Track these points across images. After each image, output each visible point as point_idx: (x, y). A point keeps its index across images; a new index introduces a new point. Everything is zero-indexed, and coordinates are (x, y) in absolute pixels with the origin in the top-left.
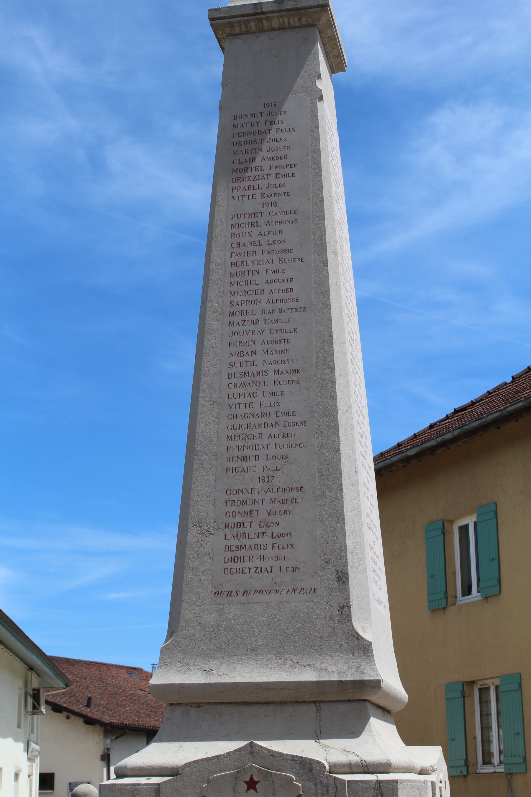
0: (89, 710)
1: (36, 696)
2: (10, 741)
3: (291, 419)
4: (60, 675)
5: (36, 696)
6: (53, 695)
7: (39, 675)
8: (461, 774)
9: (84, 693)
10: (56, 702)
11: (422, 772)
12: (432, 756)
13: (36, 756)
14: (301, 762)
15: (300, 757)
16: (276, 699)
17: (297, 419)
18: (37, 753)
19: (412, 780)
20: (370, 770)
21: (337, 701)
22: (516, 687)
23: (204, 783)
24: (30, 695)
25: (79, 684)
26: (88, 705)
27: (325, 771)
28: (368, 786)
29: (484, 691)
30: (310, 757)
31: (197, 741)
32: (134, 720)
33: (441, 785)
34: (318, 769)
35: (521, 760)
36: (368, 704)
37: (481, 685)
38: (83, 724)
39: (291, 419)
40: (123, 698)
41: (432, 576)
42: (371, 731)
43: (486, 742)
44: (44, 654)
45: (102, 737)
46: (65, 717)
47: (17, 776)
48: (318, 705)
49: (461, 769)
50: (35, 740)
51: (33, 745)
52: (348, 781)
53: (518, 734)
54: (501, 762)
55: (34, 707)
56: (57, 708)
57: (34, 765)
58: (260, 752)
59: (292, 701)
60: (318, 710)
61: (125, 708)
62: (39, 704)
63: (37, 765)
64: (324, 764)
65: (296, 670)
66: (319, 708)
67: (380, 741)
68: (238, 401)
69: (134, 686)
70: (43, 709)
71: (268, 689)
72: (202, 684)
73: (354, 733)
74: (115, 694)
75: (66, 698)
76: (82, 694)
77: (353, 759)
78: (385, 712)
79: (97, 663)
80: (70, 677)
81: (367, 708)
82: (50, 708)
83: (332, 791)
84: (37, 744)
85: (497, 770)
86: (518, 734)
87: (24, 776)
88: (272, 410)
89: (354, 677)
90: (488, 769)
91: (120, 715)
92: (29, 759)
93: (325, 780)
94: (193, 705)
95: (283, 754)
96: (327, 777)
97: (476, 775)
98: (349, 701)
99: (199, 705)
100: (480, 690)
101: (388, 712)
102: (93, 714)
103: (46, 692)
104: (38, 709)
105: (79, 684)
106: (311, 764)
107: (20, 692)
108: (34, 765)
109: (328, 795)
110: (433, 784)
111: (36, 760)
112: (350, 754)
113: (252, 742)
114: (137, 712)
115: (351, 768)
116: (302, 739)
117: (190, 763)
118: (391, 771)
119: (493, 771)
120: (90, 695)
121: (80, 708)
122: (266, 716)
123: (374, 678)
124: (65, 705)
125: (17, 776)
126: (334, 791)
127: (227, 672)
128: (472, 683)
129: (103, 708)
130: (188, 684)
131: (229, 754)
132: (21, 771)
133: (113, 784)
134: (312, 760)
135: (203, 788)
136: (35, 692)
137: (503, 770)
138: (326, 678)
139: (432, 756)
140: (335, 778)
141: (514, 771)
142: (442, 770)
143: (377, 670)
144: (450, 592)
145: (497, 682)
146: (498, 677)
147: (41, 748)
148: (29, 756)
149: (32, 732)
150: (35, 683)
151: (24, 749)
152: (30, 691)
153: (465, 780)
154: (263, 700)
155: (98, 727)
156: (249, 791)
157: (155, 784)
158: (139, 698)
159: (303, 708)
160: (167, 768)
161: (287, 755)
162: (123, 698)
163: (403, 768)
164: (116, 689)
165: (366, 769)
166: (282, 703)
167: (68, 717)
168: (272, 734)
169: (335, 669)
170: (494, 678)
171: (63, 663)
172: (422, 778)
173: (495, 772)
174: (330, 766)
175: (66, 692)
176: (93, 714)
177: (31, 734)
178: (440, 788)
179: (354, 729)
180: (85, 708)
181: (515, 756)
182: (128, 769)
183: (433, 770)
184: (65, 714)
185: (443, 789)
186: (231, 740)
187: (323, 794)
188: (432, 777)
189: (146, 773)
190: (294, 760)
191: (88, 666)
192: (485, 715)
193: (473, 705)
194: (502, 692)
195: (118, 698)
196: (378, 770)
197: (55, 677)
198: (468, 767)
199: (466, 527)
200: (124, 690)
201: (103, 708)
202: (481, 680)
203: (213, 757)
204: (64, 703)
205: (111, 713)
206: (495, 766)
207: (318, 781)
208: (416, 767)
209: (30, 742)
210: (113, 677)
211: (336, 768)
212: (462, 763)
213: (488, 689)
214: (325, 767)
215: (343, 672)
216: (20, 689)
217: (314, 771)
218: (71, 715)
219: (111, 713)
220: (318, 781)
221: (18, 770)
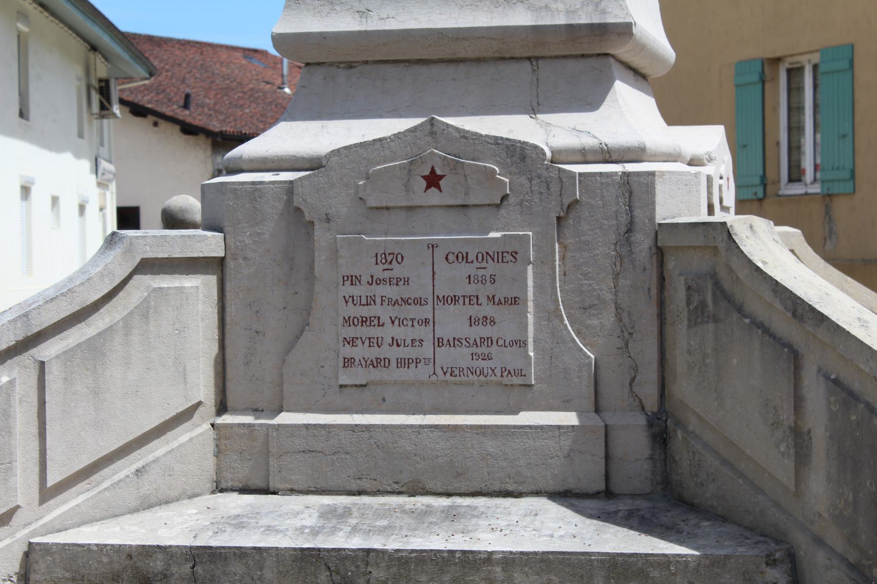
0: (187, 112)
1: (104, 90)
2: (67, 158)
4: (140, 58)
5: (104, 90)
6: (131, 90)
7: (106, 59)
8: (754, 197)
9: (179, 88)
10: (136, 101)
11: (693, 162)
12: (709, 140)
13: (109, 181)
14: (507, 147)
15: (507, 139)
16: (471, 55)
18: (110, 176)
19: (677, 172)
20: (613, 158)
21: (565, 57)
22: (845, 64)
23: (362, 179)
24: (95, 89)
25: (170, 74)
26: (186, 106)
27: (544, 160)
28: (609, 180)
29: (794, 73)
30: (522, 138)
31: (349, 118)
32: (257, 127)
33: (721, 182)
34: (534, 156)
35: (846, 175)
36: (612, 60)
37: (791, 64)
38: (180, 134)
40: (240, 95)
41: (745, 146)
42: (616, 101)
43: (795, 149)
44: (116, 29)
45: (209, 152)
46: (151, 123)
47: (82, 208)
48: (534, 63)
49: (754, 190)
50: (106, 155)
51: (104, 164)
52: (580, 174)
53: (844, 136)
54: (815, 180)
55: (103, 107)
56: (138, 110)
57: (108, 194)
58: (445, 132)
59: (494, 58)
60: (534, 71)
61: (243, 110)
62: (109, 100)
63: (112, 193)
64: (543, 150)
65: (500, 9)
66: (535, 68)
67: (628, 116)
69: (255, 77)
70: (116, 109)
71: (457, 39)
72: (354, 32)
73: (590, 104)
74: (227, 88)
75: (152, 95)
76: (176, 89)
77: (588, 142)
78: (638, 76)
79: (197, 43)
80: (155, 64)
81: (610, 66)
82: (127, 109)
83: (555, 188)
84: (110, 162)
85: (810, 191)
86: (844, 136)
87: (92, 209)
89: (591, 19)
90: (797, 189)
91: (235, 120)
92: (100, 184)
93: (545, 173)
94: (341, 66)
95: (481, 135)
96: (547, 169)
97: (778, 198)
98: (583, 56)
99: (350, 66)
100: (789, 71)
101: (644, 77)
102: (194, 118)
103: (119, 85)
104: (108, 109)
105: (170, 74)
106: (523, 149)
107: (79, 83)
108: (108, 194)
109: (549, 194)
110: (709, 179)
111: (110, 187)
112: (583, 135)
113: (433, 118)
114: (262, 115)
115: (584, 155)
116: (510, 114)
117: (338, 150)
118: (645, 158)
119: (802, 191)
120: (188, 91)
121: (173, 110)
122: (454, 80)
123: (621, 21)
124: (150, 106)
125: (82, 208)
126: (559, 189)
127: (392, 13)
128: (776, 61)
129: (209, 110)
130: (333, 33)
131: (397, 136)
132: (87, 202)
133: (222, 183)
134: (525, 143)
135: (358, 186)
136: (103, 84)
137: (818, 190)
138: (546, 20)
139: (709, 140)
140: (560, 169)
141: (836, 191)
142: (724, 161)
143: (627, 7)
144: (770, 175)
145: (816, 58)
146: (817, 51)
147: (116, 168)
148: (99, 180)
149: (102, 145)
150: (102, 70)
151: (91, 168)
152: (95, 83)
153: (761, 205)
154: (449, 57)
155: (202, 138)
156: (429, 191)
157: (286, 182)
158: (264, 95)
159: (514, 67)
160: (303, 159)
161: (487, 136)
162: (240, 95)
163: (664, 154)
164: (228, 82)
165: (607, 157)
166: (479, 60)
167: (156, 124)
168: (463, 107)
169: (561, 6)
170: (811, 52)
171: (144, 43)
172: (693, 169)
173: (806, 194)
174: (552, 152)
175: (152, 86)
176: (194, 118)
177: (100, 148)
178: (720, 187)
179: (591, 100)
180: (181, 109)
181: (838, 168)
182: (244, 161)
183: (710, 160)
184: (151, 119)
185: (724, 188)
186: (401, 116)
187: (541, 193)
188: (705, 170)
189: (272, 166)
190: (498, 144)
191: (183, 48)
192: (795, 110)
193: (776, 87)
194: (823, 73)
195: (231, 94)
196: (626, 158)
197: (132, 61)
198: (765, 186)
200: (240, 83)
201: (209, 110)
202: (792, 56)
203: (374, 140)
204: (149, 102)
205: (222, 117)
206: (806, 185)
207: (534, 174)
208: (683, 153)
209: (99, 160)
210: (222, 63)
211: (561, 155)
212: (757, 180)
213: (800, 70)
214: (544, 154)
215: (574, 12)
216: (79, 79)
217: (528, 160)
218: (160, 121)
219: (222, 117)
220: (534, 174)
221: (83, 201)
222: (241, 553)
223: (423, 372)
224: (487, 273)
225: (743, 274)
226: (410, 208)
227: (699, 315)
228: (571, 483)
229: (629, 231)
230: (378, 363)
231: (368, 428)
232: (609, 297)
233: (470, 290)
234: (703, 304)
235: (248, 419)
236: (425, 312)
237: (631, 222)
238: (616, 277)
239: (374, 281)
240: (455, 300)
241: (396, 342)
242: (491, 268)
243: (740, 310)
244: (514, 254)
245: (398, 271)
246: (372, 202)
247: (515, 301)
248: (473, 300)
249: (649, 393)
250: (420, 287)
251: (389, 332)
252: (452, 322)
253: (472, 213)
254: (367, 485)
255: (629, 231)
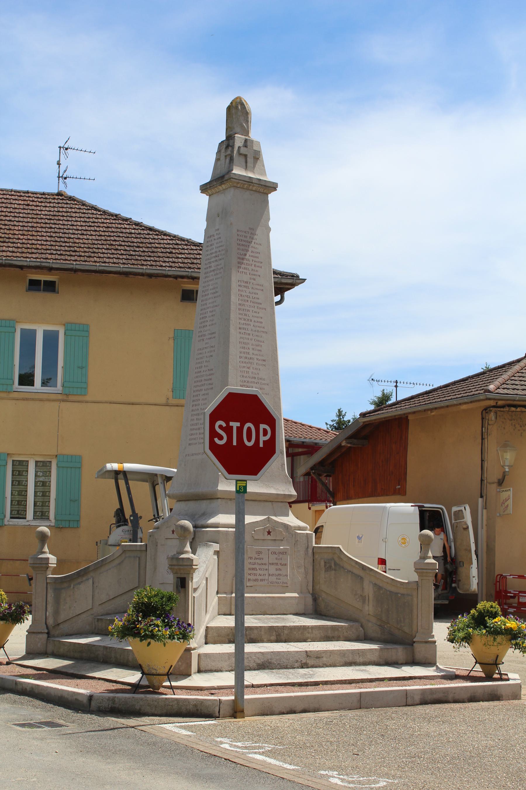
3: (263, 382)
17: (265, 382)
39: (263, 382)
68: (244, 369)
83: (294, 536)
88: (256, 376)
199: (44, 383)
222: (256, 628)
223: (266, 582)
224: (280, 557)
225: (345, 559)
226: (263, 540)
227: (328, 568)
228: (297, 611)
229: (307, 548)
230: (256, 580)
231: (255, 597)
232: (303, 564)
233: (276, 561)
234: (330, 567)
235: (225, 595)
236: (266, 567)
237: (308, 546)
238: (305, 559)
239: (256, 559)
240: (273, 564)
241: (260, 575)
242: (281, 556)
243: (343, 568)
244: (286, 553)
245: (261, 556)
246: (256, 538)
247: (286, 565)
248: (277, 564)
249: (310, 588)
250: (265, 561)
251: (259, 572)
252: (272, 570)
253: (277, 542)
254: (254, 613)
255: (307, 548)
